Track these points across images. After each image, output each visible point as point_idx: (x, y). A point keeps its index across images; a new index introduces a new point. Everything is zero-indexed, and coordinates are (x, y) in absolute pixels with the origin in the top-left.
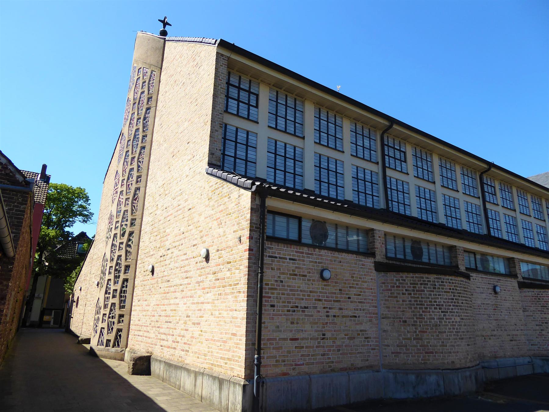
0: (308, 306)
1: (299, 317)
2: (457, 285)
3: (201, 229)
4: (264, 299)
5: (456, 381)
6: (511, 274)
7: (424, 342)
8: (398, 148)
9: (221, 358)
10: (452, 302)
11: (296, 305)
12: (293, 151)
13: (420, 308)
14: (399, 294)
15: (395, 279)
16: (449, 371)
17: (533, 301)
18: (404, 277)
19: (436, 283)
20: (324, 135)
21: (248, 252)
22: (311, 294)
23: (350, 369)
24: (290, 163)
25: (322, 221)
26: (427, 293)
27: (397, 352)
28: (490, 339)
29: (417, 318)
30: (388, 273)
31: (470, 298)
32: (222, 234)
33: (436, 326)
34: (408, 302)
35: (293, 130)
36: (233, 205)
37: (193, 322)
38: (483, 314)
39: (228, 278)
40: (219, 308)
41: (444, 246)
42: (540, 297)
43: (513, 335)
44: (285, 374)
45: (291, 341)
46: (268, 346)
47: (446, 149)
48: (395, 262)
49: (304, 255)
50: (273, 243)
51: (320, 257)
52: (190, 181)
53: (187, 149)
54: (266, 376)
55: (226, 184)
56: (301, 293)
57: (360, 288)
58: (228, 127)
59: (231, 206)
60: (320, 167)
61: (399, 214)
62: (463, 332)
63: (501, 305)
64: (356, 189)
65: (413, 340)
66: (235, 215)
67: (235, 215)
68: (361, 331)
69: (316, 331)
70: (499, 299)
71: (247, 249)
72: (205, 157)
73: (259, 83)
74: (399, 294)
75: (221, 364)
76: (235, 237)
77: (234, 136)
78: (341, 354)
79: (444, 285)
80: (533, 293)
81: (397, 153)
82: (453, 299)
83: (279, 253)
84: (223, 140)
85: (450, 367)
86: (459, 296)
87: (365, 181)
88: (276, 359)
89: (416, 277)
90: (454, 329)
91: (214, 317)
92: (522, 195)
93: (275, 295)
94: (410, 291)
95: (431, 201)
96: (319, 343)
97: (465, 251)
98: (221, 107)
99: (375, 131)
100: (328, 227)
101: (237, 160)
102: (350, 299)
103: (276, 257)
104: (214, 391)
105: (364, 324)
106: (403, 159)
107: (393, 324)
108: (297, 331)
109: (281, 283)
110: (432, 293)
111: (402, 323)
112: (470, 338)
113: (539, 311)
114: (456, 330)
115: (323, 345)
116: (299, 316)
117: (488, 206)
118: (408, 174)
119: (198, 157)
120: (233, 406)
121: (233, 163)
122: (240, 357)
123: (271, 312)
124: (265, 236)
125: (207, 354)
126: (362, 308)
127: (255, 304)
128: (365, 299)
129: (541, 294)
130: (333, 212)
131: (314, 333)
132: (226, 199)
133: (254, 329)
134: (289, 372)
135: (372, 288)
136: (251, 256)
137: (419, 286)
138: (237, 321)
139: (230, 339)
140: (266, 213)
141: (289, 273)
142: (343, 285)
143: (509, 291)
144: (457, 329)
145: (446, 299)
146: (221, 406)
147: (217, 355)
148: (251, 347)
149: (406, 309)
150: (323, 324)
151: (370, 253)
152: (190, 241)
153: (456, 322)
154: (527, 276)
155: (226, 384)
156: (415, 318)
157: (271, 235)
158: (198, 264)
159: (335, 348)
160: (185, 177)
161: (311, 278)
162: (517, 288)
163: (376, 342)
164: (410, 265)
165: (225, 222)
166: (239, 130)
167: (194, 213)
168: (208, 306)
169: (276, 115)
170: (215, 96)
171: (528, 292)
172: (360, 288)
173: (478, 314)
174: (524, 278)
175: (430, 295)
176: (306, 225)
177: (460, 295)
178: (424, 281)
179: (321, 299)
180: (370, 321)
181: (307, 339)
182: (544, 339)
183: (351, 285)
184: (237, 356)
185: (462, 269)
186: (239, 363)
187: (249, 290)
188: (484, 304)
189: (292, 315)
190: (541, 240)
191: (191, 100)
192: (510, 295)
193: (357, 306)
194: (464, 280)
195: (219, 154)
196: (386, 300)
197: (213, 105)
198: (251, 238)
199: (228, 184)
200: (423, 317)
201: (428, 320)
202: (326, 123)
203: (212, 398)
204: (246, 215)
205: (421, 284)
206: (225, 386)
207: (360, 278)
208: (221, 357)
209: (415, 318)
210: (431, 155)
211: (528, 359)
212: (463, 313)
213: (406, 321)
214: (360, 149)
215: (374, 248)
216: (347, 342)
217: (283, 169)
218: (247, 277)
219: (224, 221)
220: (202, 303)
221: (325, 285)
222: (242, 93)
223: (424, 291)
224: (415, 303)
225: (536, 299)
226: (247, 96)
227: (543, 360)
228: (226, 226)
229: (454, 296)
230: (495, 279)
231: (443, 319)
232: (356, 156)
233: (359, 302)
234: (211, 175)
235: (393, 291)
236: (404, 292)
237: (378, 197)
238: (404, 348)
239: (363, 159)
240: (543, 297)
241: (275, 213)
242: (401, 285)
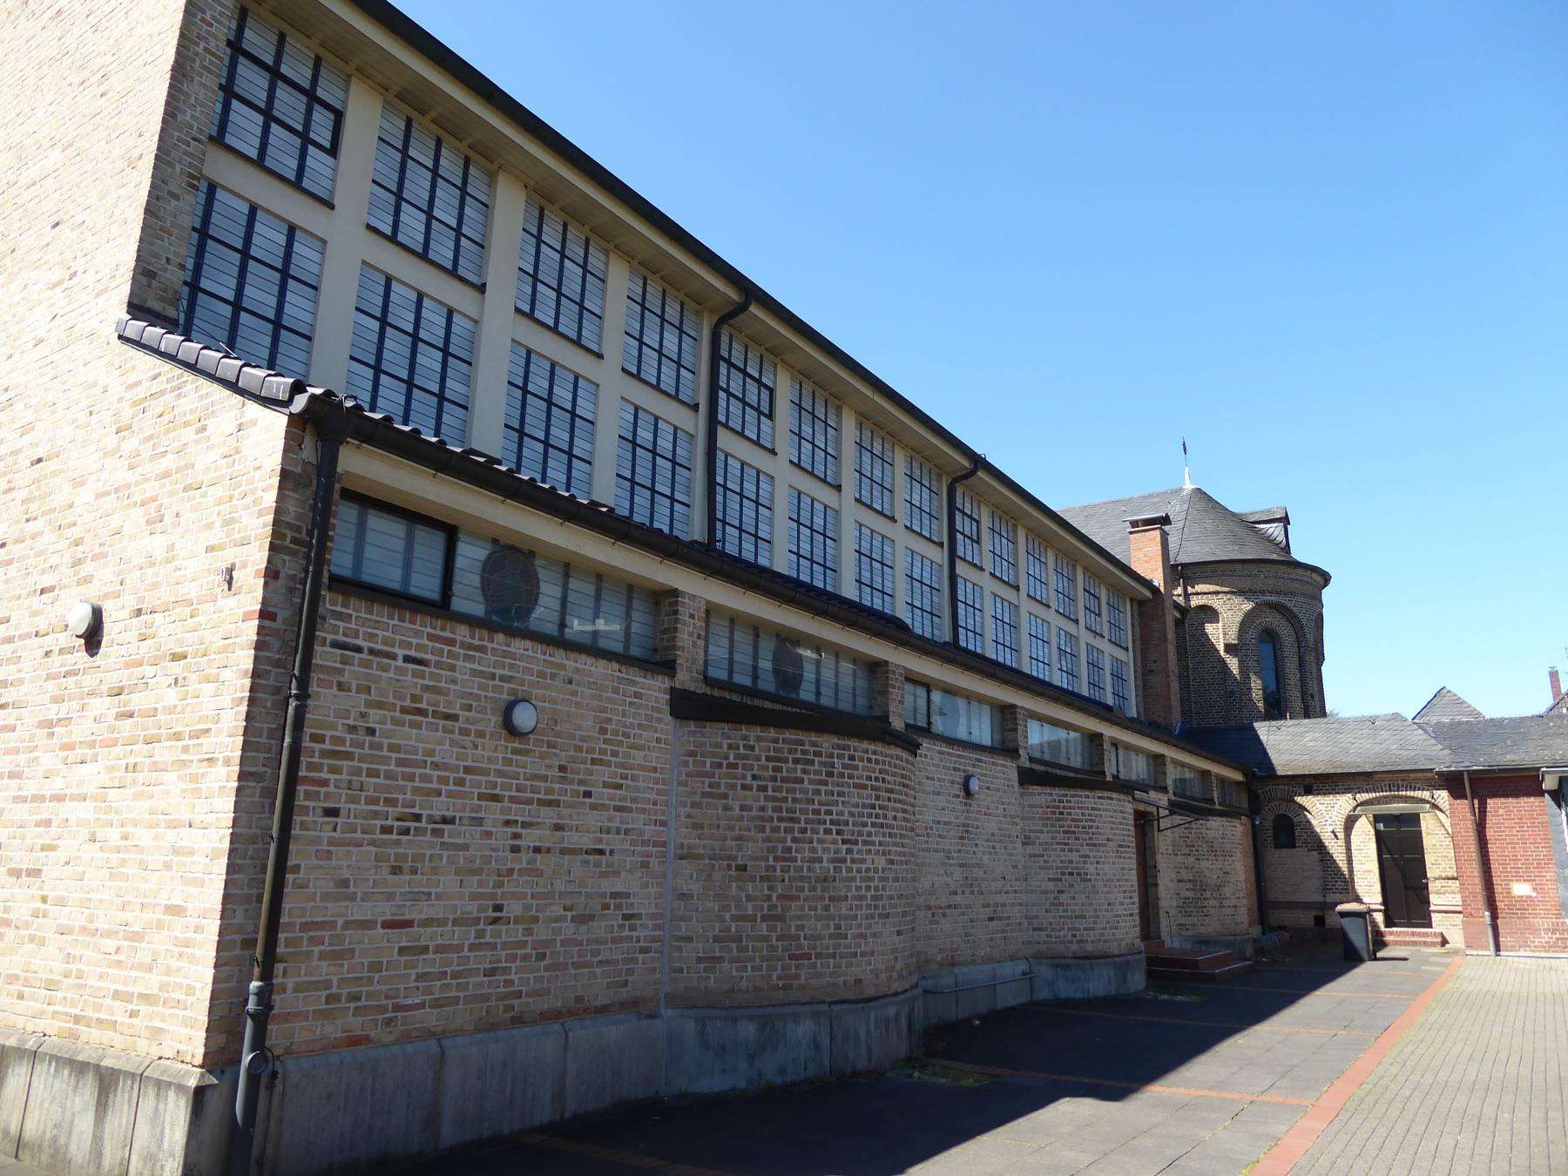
0: (454, 818)
1: (423, 851)
2: (887, 767)
3: (77, 532)
4: (301, 788)
5: (862, 1033)
6: (1006, 748)
7: (790, 926)
8: (756, 375)
9: (117, 995)
10: (870, 816)
11: (416, 811)
12: (443, 322)
13: (787, 830)
14: (733, 787)
15: (725, 743)
16: (846, 1006)
17: (1048, 819)
18: (752, 738)
19: (836, 760)
20: (547, 295)
21: (256, 622)
22: (469, 777)
23: (571, 1013)
24: (429, 360)
25: (525, 548)
26: (811, 787)
27: (714, 958)
28: (944, 915)
29: (776, 859)
30: (708, 724)
31: (913, 806)
32: (160, 554)
33: (825, 880)
34: (755, 813)
35: (450, 255)
36: (214, 455)
37: (12, 866)
38: (936, 851)
39: (171, 710)
40: (124, 816)
41: (857, 659)
42: (1064, 808)
43: (996, 905)
44: (355, 1041)
45: (386, 931)
46: (304, 949)
47: (879, 399)
48: (727, 695)
49: (456, 649)
50: (352, 601)
51: (507, 661)
52: (48, 360)
53: (48, 244)
54: (288, 1051)
55: (193, 382)
56: (436, 773)
57: (621, 765)
58: (220, 194)
59: (206, 460)
60: (525, 391)
61: (738, 560)
62: (891, 897)
63: (978, 828)
64: (628, 474)
65: (759, 919)
66: (217, 492)
67: (217, 492)
68: (614, 895)
69: (474, 897)
70: (972, 812)
71: (254, 611)
72: (119, 280)
73: (349, 76)
74: (733, 787)
75: (114, 1018)
76: (209, 570)
77: (241, 231)
78: (547, 968)
79: (856, 768)
80: (1050, 798)
81: (752, 388)
82: (873, 807)
83: (371, 637)
84: (196, 235)
85: (849, 995)
86: (889, 800)
87: (654, 453)
88: (328, 992)
89: (784, 741)
90: (868, 888)
91: (102, 849)
92: (1037, 551)
93: (344, 777)
94: (765, 780)
95: (825, 536)
96: (480, 934)
97: (908, 679)
98: (202, 116)
99: (698, 314)
100: (538, 569)
101: (244, 318)
102: (590, 797)
103: (359, 649)
104: (73, 1115)
105: (623, 874)
106: (765, 408)
107: (710, 875)
108: (409, 896)
109: (368, 738)
110: (823, 788)
111: (733, 873)
112: (905, 914)
113: (1058, 843)
114: (873, 893)
115: (493, 940)
116: (422, 848)
117: (961, 568)
118: (773, 452)
119: (90, 277)
120: (149, 1165)
121: (226, 324)
122: (190, 990)
123: (323, 834)
124: (326, 574)
125: (59, 981)
126: (624, 826)
127: (274, 747)
128: (634, 800)
129: (1067, 802)
130: (562, 524)
131: (467, 902)
132: (188, 435)
133: (255, 892)
134: (372, 1033)
135: (659, 766)
136: (268, 638)
137: (791, 765)
138: (192, 863)
139: (160, 925)
140: (336, 496)
141: (399, 703)
142: (572, 753)
143: (998, 790)
144: (876, 889)
145: (857, 805)
146: (98, 1168)
147: (100, 984)
148: (237, 952)
149: (750, 831)
150: (499, 875)
151: (660, 662)
152: (28, 574)
153: (876, 870)
154: (1037, 755)
155: (128, 1087)
156: (771, 859)
157: (347, 573)
158: (55, 657)
159: (528, 951)
160: (32, 343)
161: (472, 727)
162: (1016, 785)
163: (656, 927)
164: (768, 705)
165: (177, 515)
166: (260, 215)
167: (54, 473)
168: (84, 811)
169: (399, 197)
170: (181, 72)
171: (1040, 794)
172: (621, 765)
173: (923, 850)
174: (1031, 759)
175: (818, 792)
176: (471, 555)
177: (892, 796)
178: (804, 752)
179: (497, 795)
180: (645, 865)
181: (442, 922)
182: (1062, 914)
183: (597, 756)
184: (180, 986)
185: (897, 724)
186: (185, 1013)
187: (249, 754)
188: (939, 823)
189: (398, 843)
190: (1065, 669)
191: (84, 74)
192: (998, 802)
193: (610, 820)
194: (905, 755)
195: (175, 277)
196: (693, 805)
197: (167, 103)
198: (271, 573)
199: (202, 382)
200: (794, 854)
201: (805, 865)
202: (557, 257)
203: (62, 1141)
204: (260, 493)
205: (796, 761)
206: (122, 1098)
207: (626, 735)
208: (116, 991)
209: (771, 859)
210: (839, 409)
211: (1022, 966)
212: (895, 844)
213: (746, 866)
214: (650, 356)
215: (675, 648)
216: (568, 928)
218: (244, 708)
219: (175, 509)
220: (59, 798)
221: (515, 752)
222: (283, 93)
223: (801, 781)
224: (775, 815)
225: (1054, 813)
226: (303, 108)
227: (1055, 966)
228: (180, 530)
229: (877, 798)
230: (970, 759)
231: (844, 861)
232: (637, 377)
233: (617, 809)
234: (138, 344)
235: (717, 779)
236: (749, 781)
237: (688, 506)
238: (734, 946)
239: (657, 388)
240: (1070, 808)
241: (369, 502)
242: (740, 762)
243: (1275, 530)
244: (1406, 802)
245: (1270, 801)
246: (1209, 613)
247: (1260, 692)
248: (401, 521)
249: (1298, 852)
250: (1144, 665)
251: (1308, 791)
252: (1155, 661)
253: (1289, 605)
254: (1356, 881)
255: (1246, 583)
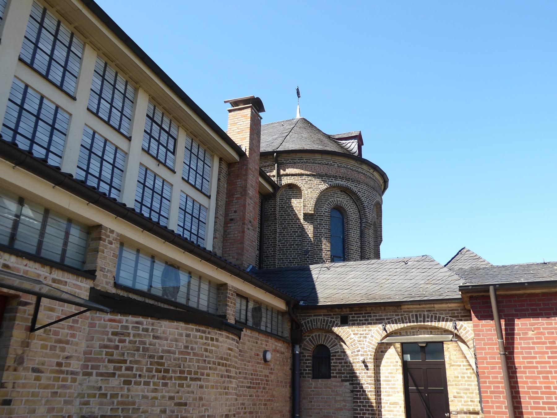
64: (140, 200)
217: (13, 127)
243: (353, 146)
244: (431, 333)
245: (311, 331)
246: (294, 190)
247: (329, 253)
248: (239, 298)
249: (333, 382)
250: (226, 214)
251: (344, 322)
252: (235, 212)
253: (355, 189)
254: (383, 413)
255: (323, 170)
